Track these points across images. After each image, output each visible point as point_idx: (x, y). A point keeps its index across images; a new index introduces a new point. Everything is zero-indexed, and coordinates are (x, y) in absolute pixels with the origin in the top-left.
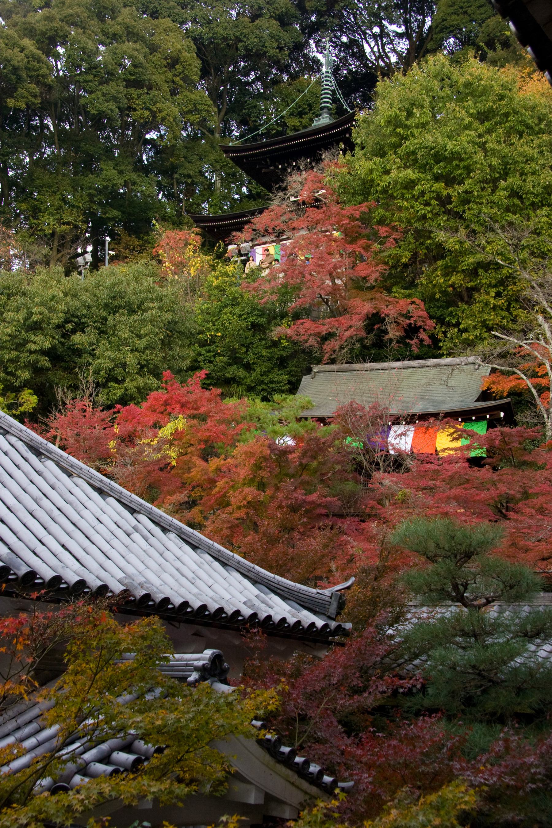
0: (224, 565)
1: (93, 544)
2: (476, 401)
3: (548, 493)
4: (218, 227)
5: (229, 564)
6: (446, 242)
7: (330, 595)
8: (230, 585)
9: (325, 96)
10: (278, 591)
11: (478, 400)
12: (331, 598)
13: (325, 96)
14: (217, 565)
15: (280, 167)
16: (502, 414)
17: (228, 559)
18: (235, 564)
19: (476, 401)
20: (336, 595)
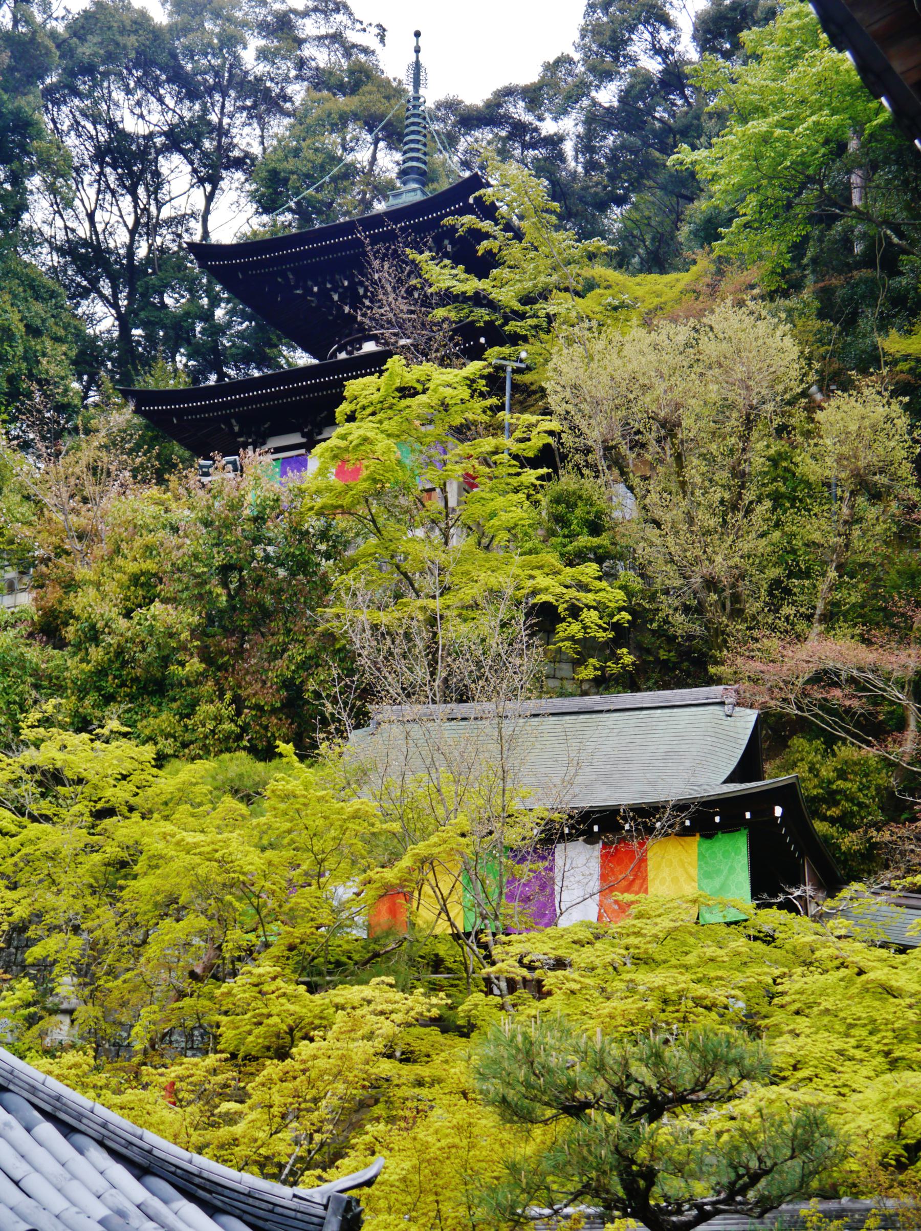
0: (67, 1130)
1: (41, 1145)
2: (725, 782)
3: (918, 992)
4: (179, 413)
5: (82, 1127)
6: (31, 192)
7: (325, 1202)
8: (74, 1177)
9: (412, 146)
10: (201, 1193)
11: (730, 780)
12: (326, 1207)
13: (412, 146)
14: (46, 1129)
15: (316, 289)
16: (778, 811)
17: (79, 1117)
18: (95, 1129)
19: (725, 782)
20: (338, 1200)
